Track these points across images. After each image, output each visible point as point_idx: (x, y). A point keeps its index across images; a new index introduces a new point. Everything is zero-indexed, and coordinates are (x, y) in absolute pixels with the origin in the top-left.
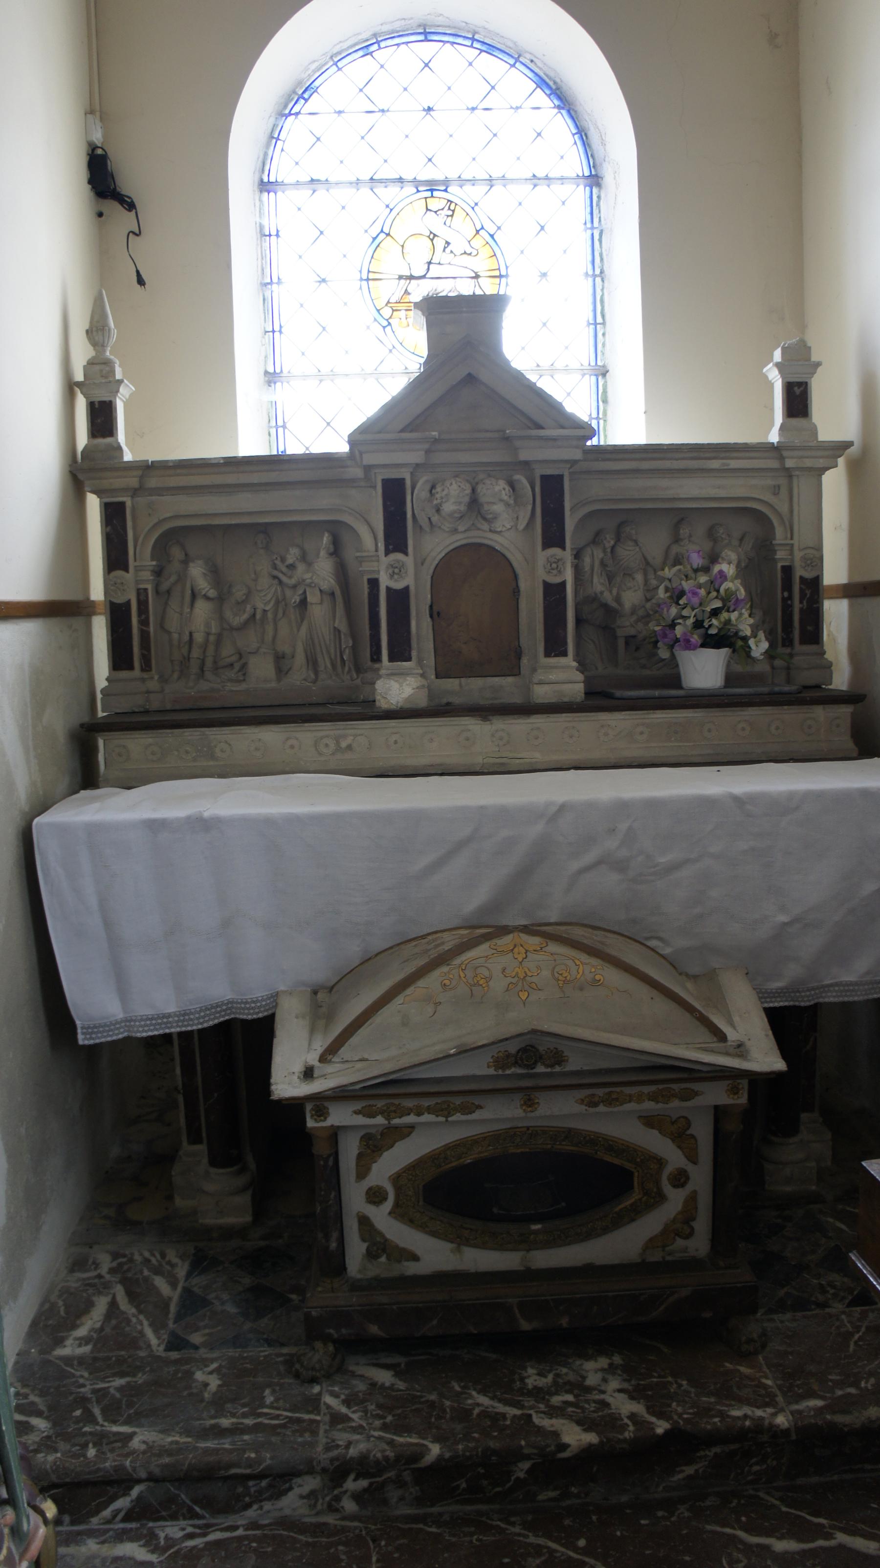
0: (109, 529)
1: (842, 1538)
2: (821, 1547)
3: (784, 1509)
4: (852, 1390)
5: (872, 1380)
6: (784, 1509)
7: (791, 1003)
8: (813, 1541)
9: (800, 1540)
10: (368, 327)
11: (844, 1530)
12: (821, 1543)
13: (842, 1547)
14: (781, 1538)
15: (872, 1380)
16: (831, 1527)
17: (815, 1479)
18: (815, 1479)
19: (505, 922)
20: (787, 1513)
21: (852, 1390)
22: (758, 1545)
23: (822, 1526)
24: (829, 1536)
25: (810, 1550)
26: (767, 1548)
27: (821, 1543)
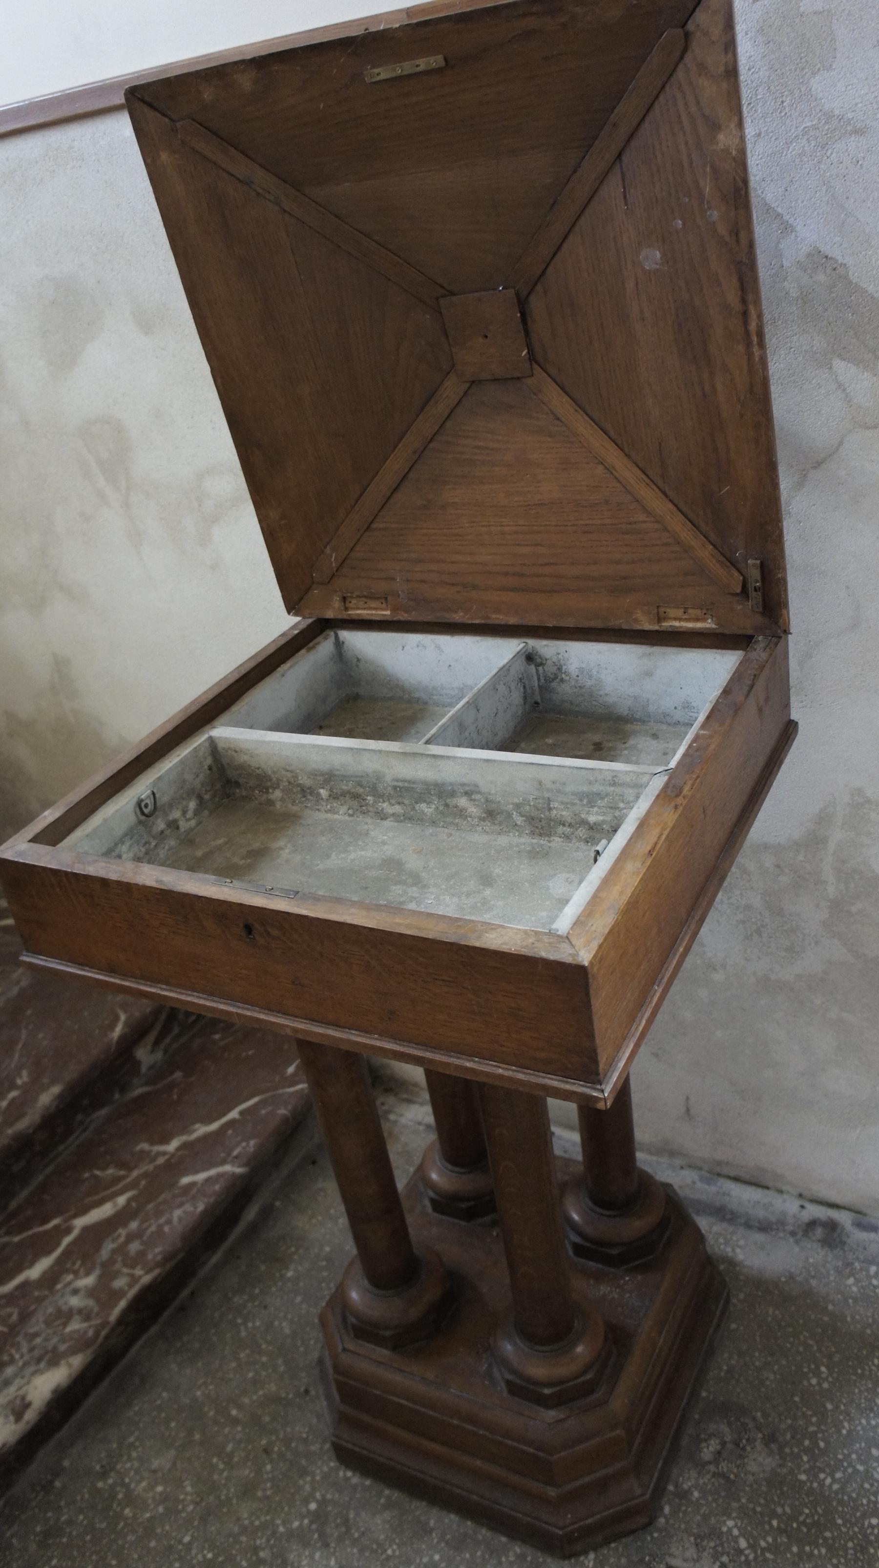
0: (273, 514)
1: (80, 1223)
2: (69, 1245)
3: (16, 1239)
4: (13, 1094)
5: (25, 1073)
6: (16, 1239)
7: (483, 622)
8: (58, 1244)
9: (49, 1253)
10: (846, 786)
11: (76, 1215)
12: (66, 1241)
13: (86, 1230)
14: (31, 1264)
15: (25, 1073)
16: (66, 1221)
17: (24, 1194)
18: (24, 1194)
19: (330, 614)
20: (22, 1241)
21: (13, 1094)
22: (17, 1288)
23: (56, 1227)
24: (69, 1230)
25: (63, 1253)
26: (25, 1284)
27: (66, 1241)
